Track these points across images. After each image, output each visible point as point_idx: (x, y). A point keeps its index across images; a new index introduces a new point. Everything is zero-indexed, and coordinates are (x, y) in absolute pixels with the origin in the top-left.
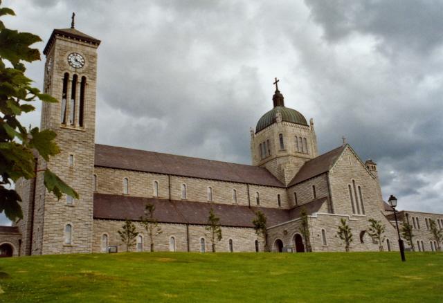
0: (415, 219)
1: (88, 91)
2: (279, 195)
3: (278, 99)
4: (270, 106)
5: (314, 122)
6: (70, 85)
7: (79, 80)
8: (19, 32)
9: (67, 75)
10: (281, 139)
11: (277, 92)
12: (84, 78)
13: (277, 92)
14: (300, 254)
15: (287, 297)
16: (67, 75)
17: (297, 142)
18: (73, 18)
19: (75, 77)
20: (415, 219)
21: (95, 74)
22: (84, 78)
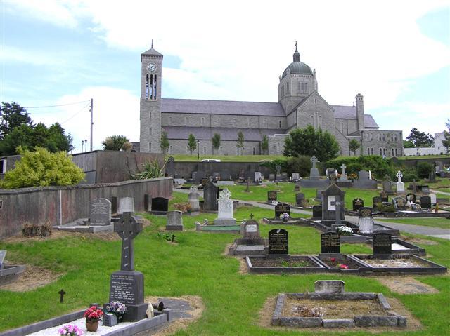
0: (370, 150)
1: (158, 81)
2: (280, 122)
3: (296, 57)
4: (291, 60)
5: (316, 71)
6: (150, 80)
7: (154, 77)
8: (48, 126)
9: (148, 75)
10: (288, 86)
11: (296, 51)
12: (156, 76)
13: (296, 51)
14: (90, 334)
15: (363, 120)
16: (148, 75)
17: (299, 86)
18: (92, 102)
19: (152, 76)
20: (370, 150)
21: (161, 73)
22: (156, 76)
